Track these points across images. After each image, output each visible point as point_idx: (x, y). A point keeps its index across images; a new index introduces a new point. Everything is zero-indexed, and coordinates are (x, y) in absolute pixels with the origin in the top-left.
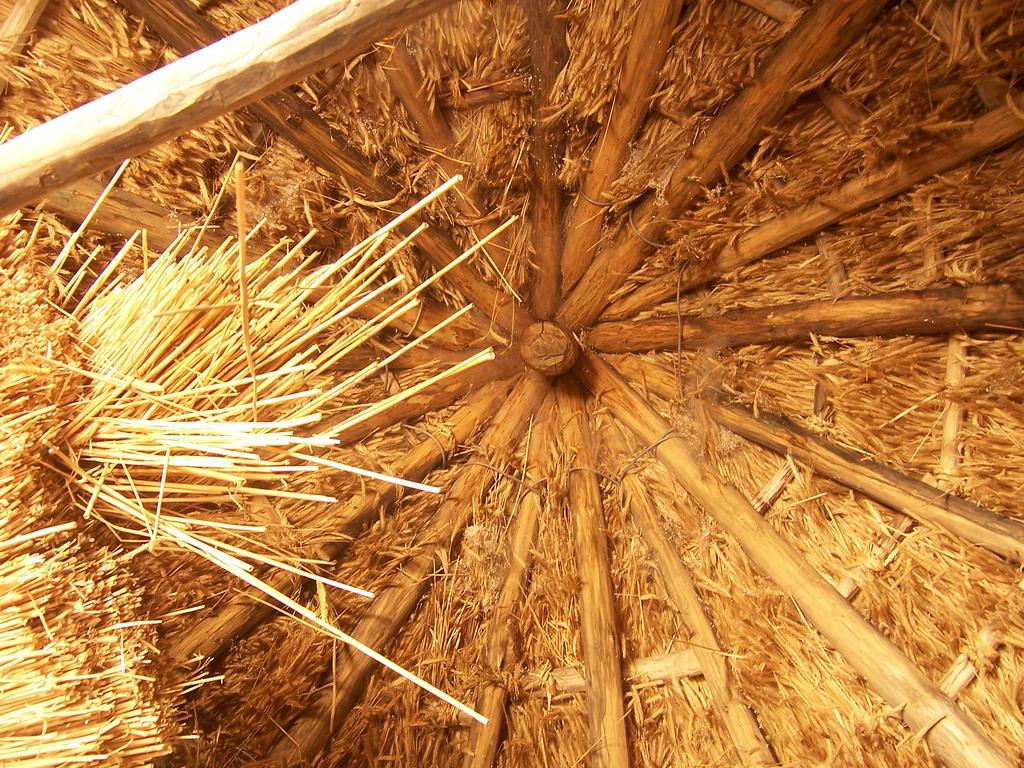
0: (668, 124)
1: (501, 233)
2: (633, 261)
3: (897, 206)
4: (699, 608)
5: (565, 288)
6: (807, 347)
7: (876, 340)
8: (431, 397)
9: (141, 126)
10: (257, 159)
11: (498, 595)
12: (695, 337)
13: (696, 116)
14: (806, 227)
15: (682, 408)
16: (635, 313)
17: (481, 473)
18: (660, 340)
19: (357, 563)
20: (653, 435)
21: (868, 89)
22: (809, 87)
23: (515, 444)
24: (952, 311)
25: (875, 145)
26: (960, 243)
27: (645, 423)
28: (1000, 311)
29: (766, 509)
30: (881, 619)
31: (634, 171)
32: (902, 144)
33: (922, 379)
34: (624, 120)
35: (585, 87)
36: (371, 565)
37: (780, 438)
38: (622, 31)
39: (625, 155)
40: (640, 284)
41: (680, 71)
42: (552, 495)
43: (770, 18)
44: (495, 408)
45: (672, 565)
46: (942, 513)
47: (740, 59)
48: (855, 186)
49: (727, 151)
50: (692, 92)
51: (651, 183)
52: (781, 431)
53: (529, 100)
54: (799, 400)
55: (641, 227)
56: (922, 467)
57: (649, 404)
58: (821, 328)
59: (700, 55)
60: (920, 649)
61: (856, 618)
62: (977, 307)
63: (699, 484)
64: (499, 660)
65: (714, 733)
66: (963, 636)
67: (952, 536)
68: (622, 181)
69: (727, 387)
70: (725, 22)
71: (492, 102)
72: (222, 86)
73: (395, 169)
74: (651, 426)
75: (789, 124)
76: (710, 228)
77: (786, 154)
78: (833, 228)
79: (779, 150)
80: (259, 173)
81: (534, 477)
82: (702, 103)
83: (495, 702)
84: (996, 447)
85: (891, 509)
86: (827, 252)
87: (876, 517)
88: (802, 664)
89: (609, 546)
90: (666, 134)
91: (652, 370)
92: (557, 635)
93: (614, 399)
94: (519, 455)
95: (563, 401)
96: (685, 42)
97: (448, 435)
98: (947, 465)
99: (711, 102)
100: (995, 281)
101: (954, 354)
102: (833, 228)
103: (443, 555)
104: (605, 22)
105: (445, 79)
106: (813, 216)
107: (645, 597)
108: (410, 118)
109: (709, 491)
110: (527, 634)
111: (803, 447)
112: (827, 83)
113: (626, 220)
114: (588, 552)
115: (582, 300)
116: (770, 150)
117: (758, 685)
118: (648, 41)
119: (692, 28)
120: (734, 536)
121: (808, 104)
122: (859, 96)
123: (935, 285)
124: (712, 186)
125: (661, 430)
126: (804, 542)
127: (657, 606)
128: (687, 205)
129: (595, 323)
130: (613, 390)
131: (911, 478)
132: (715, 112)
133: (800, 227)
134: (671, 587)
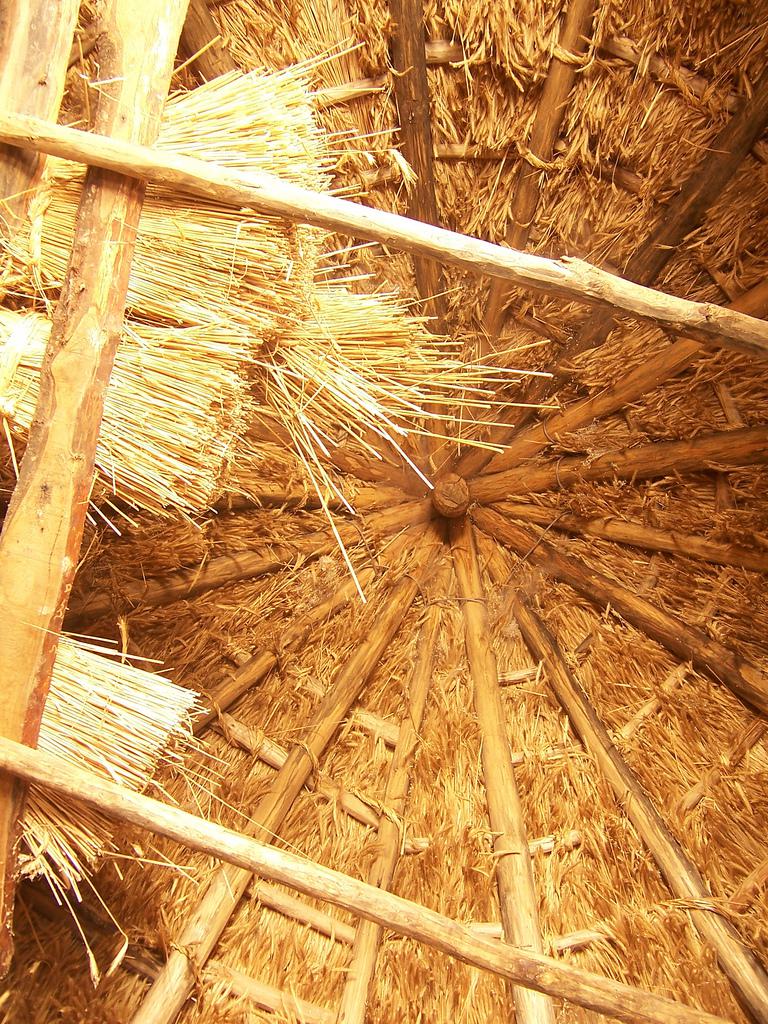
0: (624, 426)
1: (478, 408)
2: (540, 486)
3: (710, 568)
4: (421, 707)
5: (486, 470)
6: (600, 612)
7: (642, 634)
8: (359, 466)
9: (446, 252)
10: (389, 254)
11: (309, 607)
12: (541, 557)
13: (643, 434)
14: (653, 542)
15: (499, 588)
16: (516, 517)
17: (354, 533)
18: (518, 543)
19: (250, 522)
20: (472, 593)
21: (746, 495)
22: (715, 468)
23: (387, 533)
24: (695, 647)
25: (724, 525)
26: (727, 614)
27: (470, 584)
28: (719, 664)
29: (503, 684)
30: (524, 784)
31: (584, 436)
32: (739, 536)
33: (650, 675)
34: (603, 404)
35: (597, 368)
36: (256, 530)
37: (544, 649)
38: (642, 355)
39: (586, 423)
40: (532, 502)
41: (656, 402)
42: (385, 578)
43: (724, 415)
44: (389, 504)
45: (424, 669)
46: (603, 752)
47: (691, 423)
48: (697, 541)
49: (645, 466)
50: (652, 419)
51: (589, 450)
52: (548, 646)
53: (560, 349)
54: (572, 637)
55: (563, 470)
56: (611, 724)
57: (481, 577)
58: (617, 604)
59: (673, 403)
60: (533, 814)
61: (510, 777)
62: (709, 653)
63: (477, 642)
64: (288, 641)
65: (378, 778)
66: (562, 826)
67: (598, 769)
68: (573, 435)
69: (537, 597)
70: (700, 398)
71: (537, 332)
72: (490, 265)
73: (454, 322)
74: (472, 588)
75: (690, 480)
76: (600, 501)
77: (675, 495)
78: (668, 555)
79: (673, 489)
80: (383, 263)
81: (381, 561)
82: (653, 430)
83: (267, 662)
84: (660, 737)
85: (576, 734)
86: (654, 566)
87: (565, 736)
88: (459, 777)
89: (395, 634)
90: (618, 430)
91: (499, 558)
92: (325, 658)
93: (463, 557)
94: (383, 542)
95: (429, 533)
96: (671, 390)
97: (353, 496)
98: (626, 731)
99: (658, 433)
100: (730, 647)
101: (678, 673)
102: (668, 555)
103: (301, 560)
104: (637, 343)
105: (524, 298)
106: (662, 540)
107: (395, 677)
108: (487, 303)
109: (479, 648)
110: (312, 643)
111: (554, 663)
112: (727, 473)
113: (556, 459)
114: (383, 625)
115: (490, 485)
116: (667, 485)
117: (426, 770)
118: (651, 373)
119: (680, 385)
120: (475, 683)
121: (709, 477)
122: (738, 495)
123: (698, 628)
124: (621, 478)
125: (477, 593)
126: (512, 717)
127: (397, 688)
128: (598, 478)
129: (486, 505)
130: (466, 551)
131: (604, 725)
132: (656, 441)
133: (651, 540)
134: (414, 683)
